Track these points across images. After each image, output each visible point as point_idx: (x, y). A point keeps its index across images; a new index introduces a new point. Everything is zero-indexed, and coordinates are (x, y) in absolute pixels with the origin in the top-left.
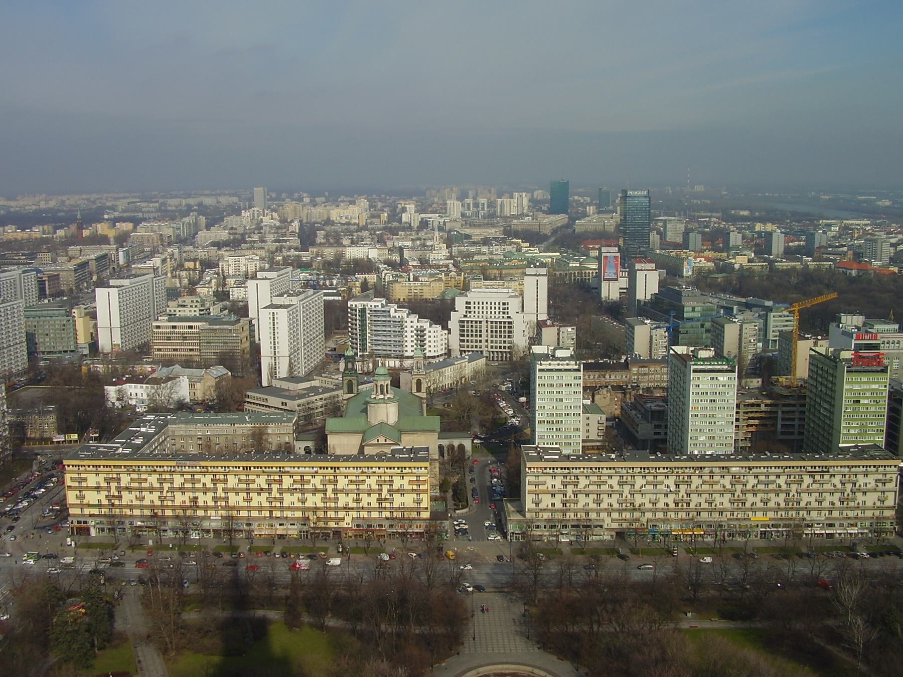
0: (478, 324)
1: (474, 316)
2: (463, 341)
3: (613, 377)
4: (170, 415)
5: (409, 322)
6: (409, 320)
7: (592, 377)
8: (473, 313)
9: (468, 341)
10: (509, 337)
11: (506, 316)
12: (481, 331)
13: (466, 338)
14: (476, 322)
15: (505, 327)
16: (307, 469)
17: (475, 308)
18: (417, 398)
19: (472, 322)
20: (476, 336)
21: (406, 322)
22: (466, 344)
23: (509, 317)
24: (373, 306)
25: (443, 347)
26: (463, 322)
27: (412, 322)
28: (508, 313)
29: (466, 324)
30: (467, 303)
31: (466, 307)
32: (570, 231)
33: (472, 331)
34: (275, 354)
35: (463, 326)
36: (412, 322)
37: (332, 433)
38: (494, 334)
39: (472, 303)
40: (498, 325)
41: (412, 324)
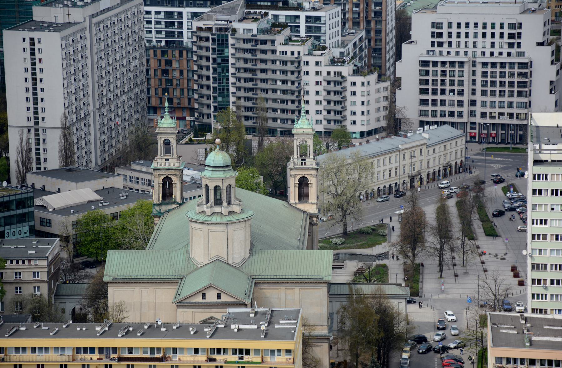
0: (457, 69)
1: (449, 53)
2: (424, 102)
6: (312, 60)
8: (446, 45)
9: (434, 102)
10: (520, 94)
11: (514, 51)
12: (461, 83)
13: (430, 97)
14: (452, 64)
16: (29, 353)
17: (450, 34)
18: (301, 215)
19: (444, 63)
20: (502, 93)
21: (307, 63)
22: (430, 108)
23: (521, 54)
24: (332, 74)
25: (383, 113)
27: (317, 63)
30: (434, 25)
31: (433, 34)
33: (443, 82)
34: (37, 123)
36: (317, 63)
37: (117, 281)
38: (489, 89)
39: (445, 26)
41: (318, 69)
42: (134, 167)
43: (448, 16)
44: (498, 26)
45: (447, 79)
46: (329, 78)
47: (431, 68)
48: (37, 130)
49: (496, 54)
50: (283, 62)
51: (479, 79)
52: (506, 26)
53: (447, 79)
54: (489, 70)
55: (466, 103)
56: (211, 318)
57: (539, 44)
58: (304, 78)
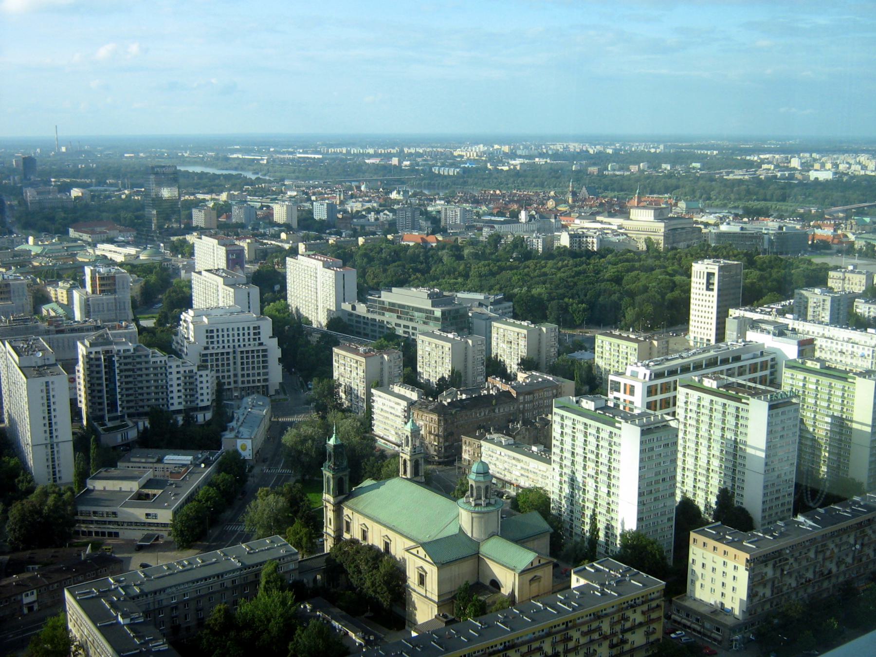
3: (502, 410)
4: (53, 244)
5: (174, 366)
7: (483, 414)
8: (216, 343)
10: (264, 367)
11: (257, 342)
15: (258, 356)
17: (218, 336)
26: (206, 355)
28: (259, 339)
29: (209, 358)
31: (259, 333)
32: (693, 205)
35: (206, 361)
39: (215, 331)
40: (250, 355)
42: (133, 459)
43: (215, 325)
44: (241, 329)
45: (220, 363)
46: (185, 375)
47: (209, 358)
48: (52, 445)
49: (242, 346)
50: (155, 368)
51: (231, 362)
52: (251, 328)
53: (220, 363)
54: (245, 355)
55: (232, 376)
56: (535, 576)
57: (270, 337)
58: (170, 376)
